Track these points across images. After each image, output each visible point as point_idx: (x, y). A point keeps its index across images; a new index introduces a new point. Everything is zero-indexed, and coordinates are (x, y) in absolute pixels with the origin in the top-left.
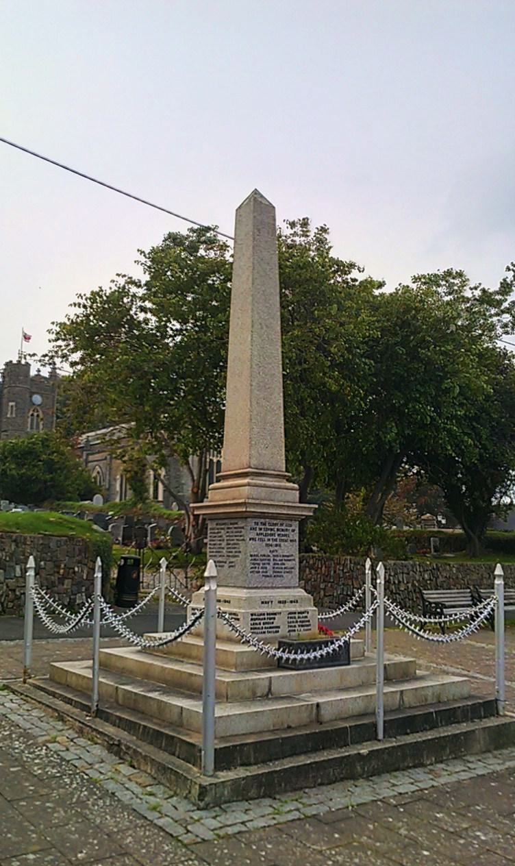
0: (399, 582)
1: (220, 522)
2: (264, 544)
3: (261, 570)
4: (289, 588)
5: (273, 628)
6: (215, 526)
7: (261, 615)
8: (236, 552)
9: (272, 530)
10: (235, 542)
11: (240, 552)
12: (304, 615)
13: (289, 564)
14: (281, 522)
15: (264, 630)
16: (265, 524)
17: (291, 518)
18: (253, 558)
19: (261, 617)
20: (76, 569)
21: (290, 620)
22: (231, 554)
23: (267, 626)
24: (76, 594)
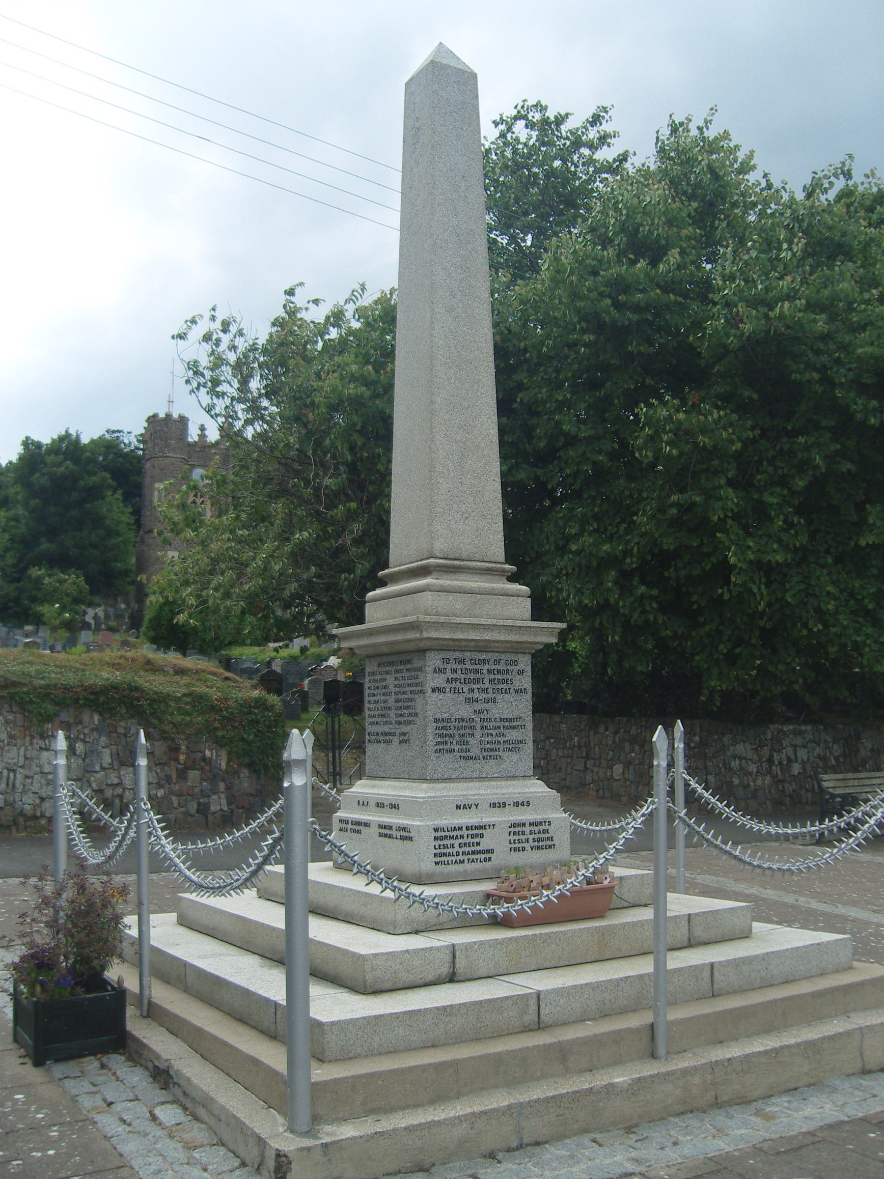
0: (789, 760)
1: (384, 659)
2: (461, 698)
3: (456, 748)
4: (514, 777)
5: (478, 852)
6: (375, 668)
7: (455, 829)
8: (410, 715)
9: (477, 671)
10: (409, 696)
11: (416, 714)
12: (541, 828)
13: (512, 735)
14: (495, 656)
15: (461, 857)
16: (462, 661)
17: (516, 648)
18: (440, 725)
19: (455, 833)
20: (208, 753)
21: (512, 838)
22: (402, 719)
23: (467, 849)
24: (209, 796)
